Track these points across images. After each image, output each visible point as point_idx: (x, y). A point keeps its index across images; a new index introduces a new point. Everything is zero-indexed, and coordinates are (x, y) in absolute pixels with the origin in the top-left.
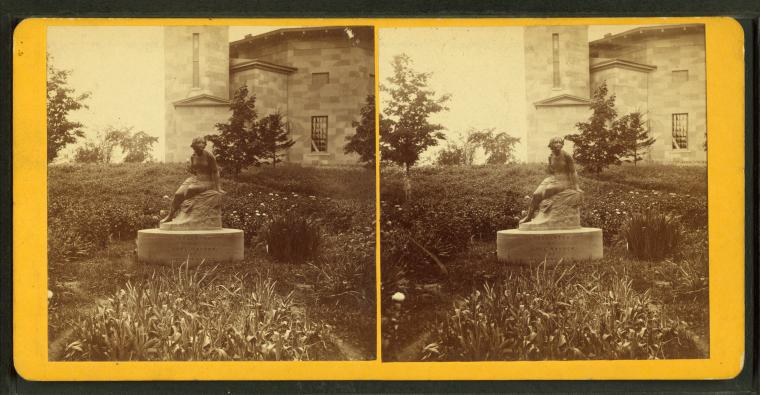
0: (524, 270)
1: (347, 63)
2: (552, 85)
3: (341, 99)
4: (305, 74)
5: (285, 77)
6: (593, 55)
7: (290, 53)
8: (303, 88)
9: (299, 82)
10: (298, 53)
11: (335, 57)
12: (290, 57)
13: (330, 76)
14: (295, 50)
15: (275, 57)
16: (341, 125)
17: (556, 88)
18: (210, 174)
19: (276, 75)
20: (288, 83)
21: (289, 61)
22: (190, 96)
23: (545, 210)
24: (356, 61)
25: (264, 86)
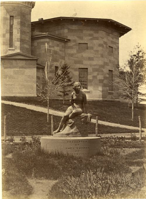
0: (22, 174)
1: (97, 38)
2: (9, 46)
3: (95, 59)
4: (74, 43)
5: (63, 44)
6: (33, 30)
7: (66, 31)
8: (74, 51)
9: (71, 48)
10: (70, 31)
11: (90, 35)
12: (65, 32)
13: (88, 45)
14: (69, 29)
15: (57, 32)
16: (95, 74)
17: (11, 48)
18: (82, 104)
19: (58, 43)
20: (64, 47)
21: (65, 35)
22: (7, 54)
23: (70, 125)
24: (102, 38)
25: (52, 49)
